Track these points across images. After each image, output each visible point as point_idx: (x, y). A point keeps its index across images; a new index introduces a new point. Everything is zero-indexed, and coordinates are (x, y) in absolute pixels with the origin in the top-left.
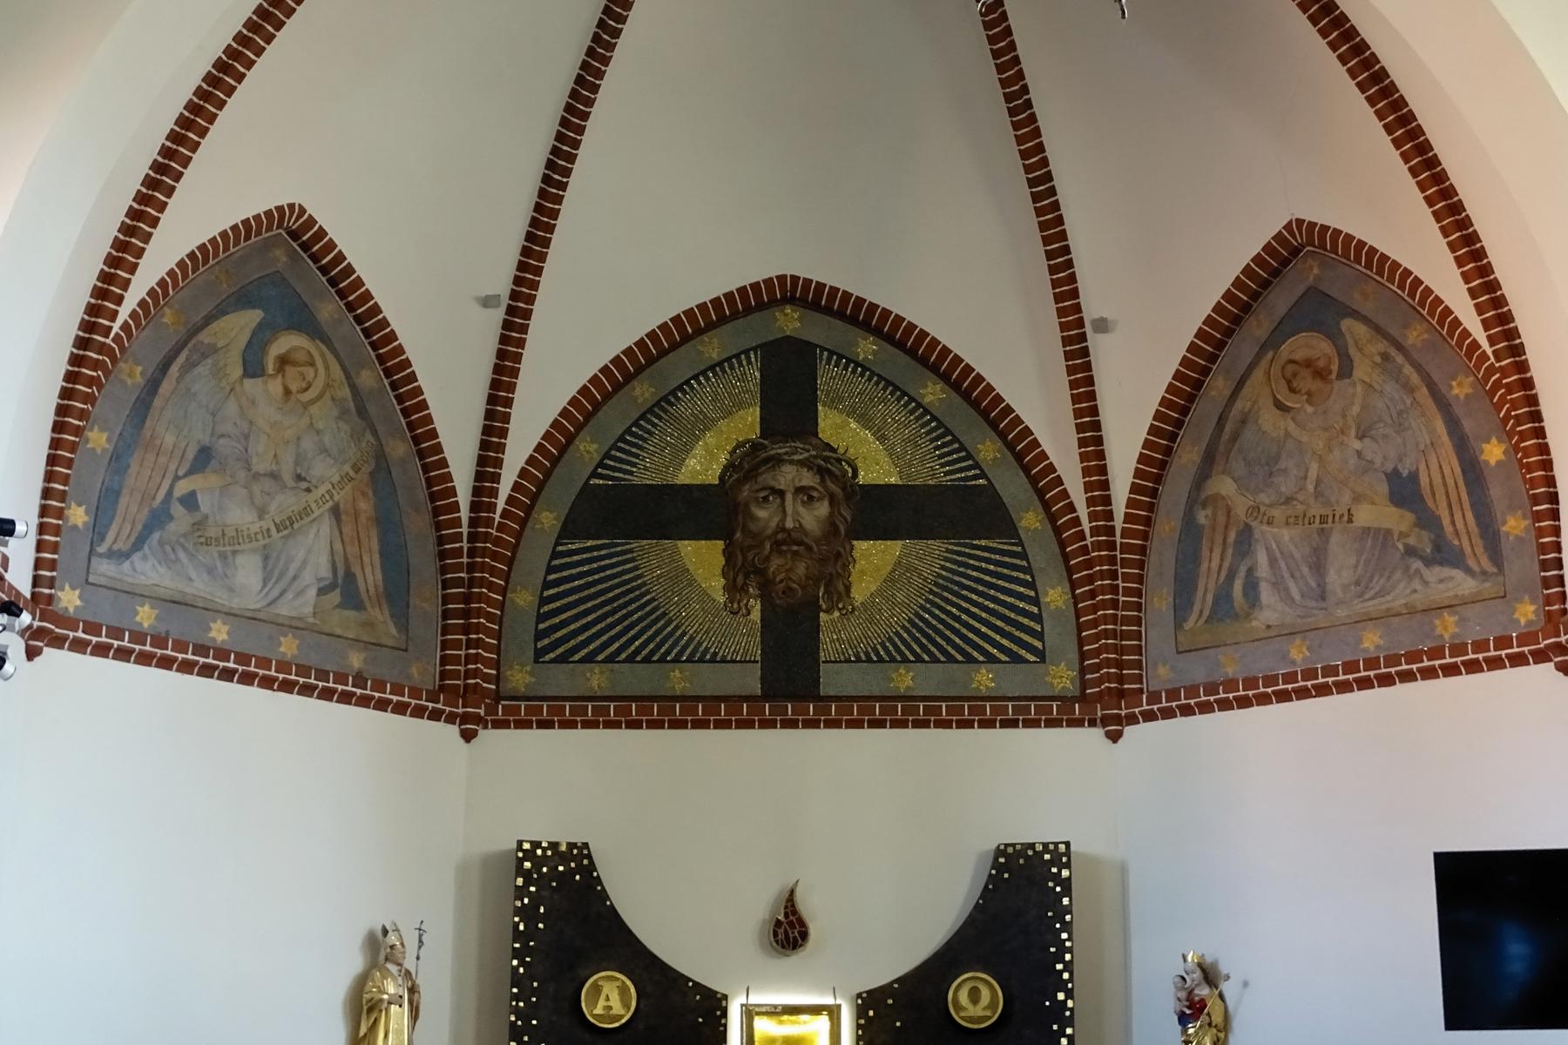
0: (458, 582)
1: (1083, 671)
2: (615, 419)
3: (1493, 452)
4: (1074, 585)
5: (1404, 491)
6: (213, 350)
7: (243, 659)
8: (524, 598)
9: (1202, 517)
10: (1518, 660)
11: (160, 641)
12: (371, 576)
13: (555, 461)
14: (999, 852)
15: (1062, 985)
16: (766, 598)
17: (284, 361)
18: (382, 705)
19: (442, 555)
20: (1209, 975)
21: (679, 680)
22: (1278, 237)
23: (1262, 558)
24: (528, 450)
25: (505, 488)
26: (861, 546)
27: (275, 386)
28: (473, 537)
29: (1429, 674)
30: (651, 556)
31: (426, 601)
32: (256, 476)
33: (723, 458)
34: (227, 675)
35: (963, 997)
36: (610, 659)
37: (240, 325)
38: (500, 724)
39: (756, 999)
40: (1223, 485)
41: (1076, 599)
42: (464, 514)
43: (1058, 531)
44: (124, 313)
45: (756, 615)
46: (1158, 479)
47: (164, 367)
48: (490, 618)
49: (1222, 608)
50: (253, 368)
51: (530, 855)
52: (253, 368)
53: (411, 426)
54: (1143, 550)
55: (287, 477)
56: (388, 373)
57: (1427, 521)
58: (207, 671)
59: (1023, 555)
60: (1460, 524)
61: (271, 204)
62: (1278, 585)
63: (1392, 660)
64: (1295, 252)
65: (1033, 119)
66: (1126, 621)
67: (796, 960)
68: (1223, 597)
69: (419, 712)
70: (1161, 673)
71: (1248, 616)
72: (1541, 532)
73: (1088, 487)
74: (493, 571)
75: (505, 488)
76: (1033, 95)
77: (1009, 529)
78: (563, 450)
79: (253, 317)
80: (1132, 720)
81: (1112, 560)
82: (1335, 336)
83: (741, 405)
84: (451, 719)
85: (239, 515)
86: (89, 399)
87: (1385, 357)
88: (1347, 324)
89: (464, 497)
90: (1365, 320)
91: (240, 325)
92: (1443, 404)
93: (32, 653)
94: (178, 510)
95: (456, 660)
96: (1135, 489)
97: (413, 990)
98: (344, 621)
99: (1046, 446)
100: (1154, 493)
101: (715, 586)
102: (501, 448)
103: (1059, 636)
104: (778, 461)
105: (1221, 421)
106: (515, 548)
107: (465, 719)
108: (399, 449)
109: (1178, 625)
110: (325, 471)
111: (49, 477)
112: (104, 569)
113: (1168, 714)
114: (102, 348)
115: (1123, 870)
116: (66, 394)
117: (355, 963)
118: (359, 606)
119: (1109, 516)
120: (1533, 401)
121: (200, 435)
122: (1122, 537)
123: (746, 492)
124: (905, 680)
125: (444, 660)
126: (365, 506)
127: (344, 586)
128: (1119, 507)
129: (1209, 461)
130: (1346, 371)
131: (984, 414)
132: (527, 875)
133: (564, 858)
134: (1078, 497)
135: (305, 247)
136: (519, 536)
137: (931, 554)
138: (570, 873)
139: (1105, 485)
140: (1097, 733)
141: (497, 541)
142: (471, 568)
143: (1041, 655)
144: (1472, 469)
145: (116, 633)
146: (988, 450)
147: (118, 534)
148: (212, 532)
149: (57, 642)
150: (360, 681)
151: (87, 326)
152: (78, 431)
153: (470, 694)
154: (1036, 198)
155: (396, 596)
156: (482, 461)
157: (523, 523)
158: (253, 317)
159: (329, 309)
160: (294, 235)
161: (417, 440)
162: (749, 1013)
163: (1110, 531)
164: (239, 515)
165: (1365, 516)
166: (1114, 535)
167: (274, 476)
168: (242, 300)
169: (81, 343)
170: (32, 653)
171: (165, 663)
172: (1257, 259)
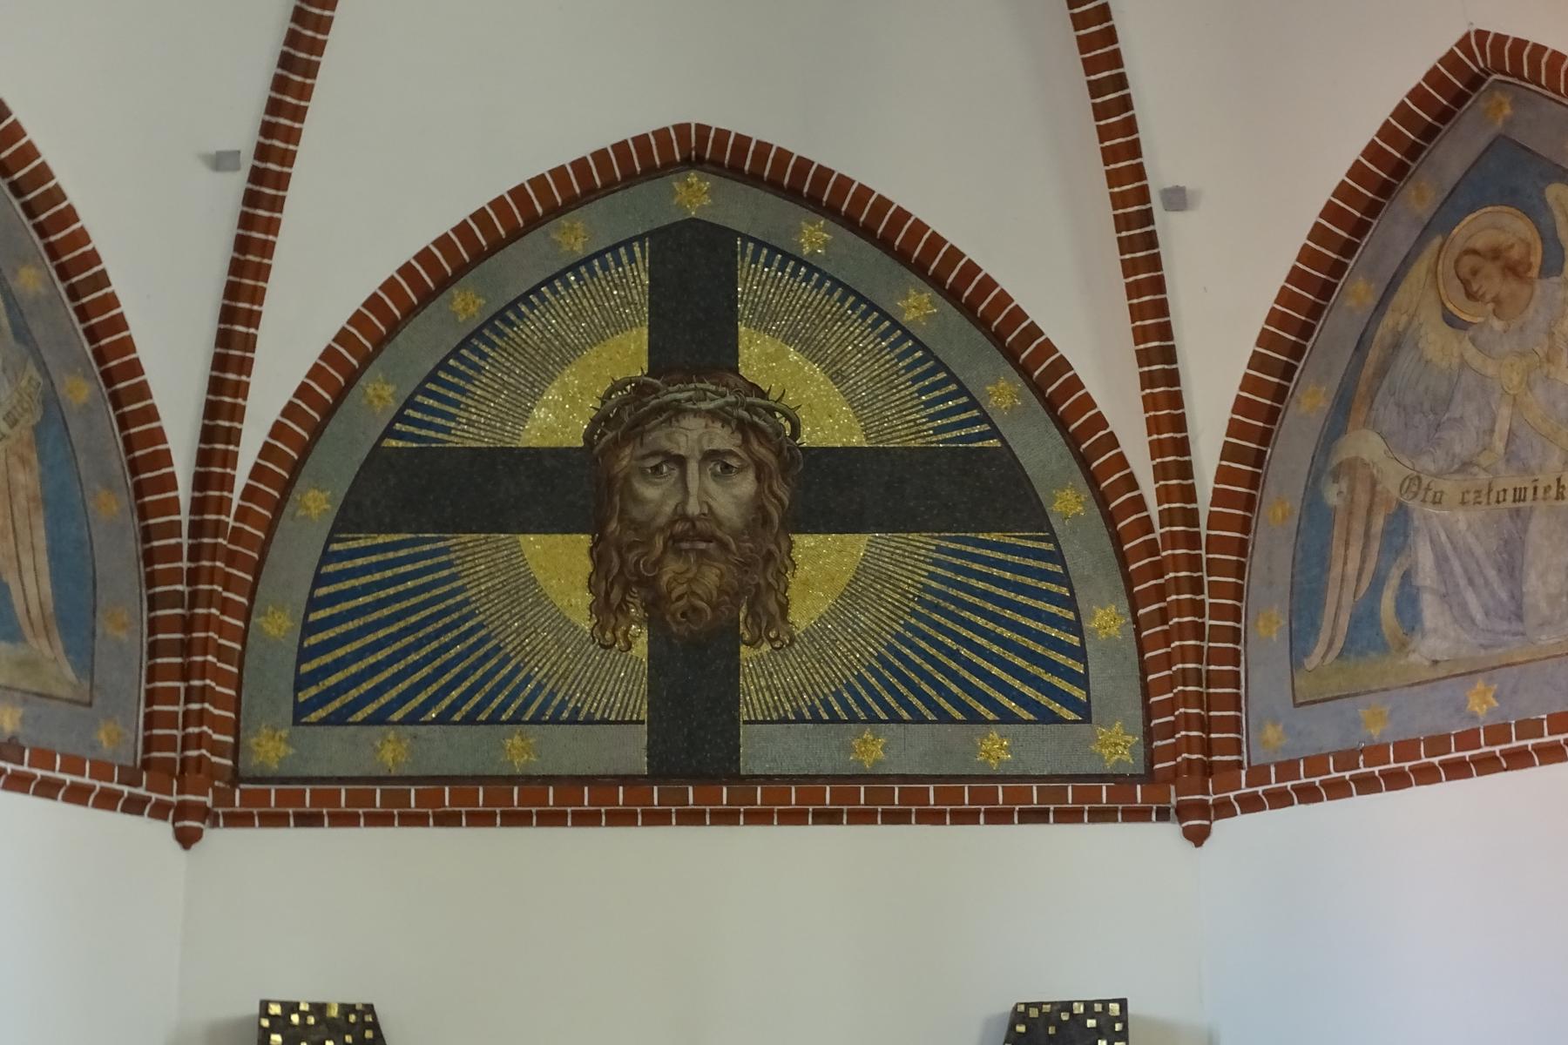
0: (174, 599)
1: (1149, 735)
9: (1333, 495)
14: (1018, 1016)
16: (656, 624)
19: (149, 557)
22: (1450, 60)
23: (1425, 558)
24: (286, 394)
25: (248, 452)
28: (197, 529)
33: (591, 405)
36: (412, 719)
38: (238, 820)
40: (1364, 445)
42: (184, 492)
45: (641, 648)
46: (1265, 437)
51: (280, 1024)
54: (1242, 548)
59: (1057, 557)
62: (1447, 597)
64: (1475, 82)
66: (1216, 656)
68: (1365, 618)
69: (107, 801)
75: (248, 452)
77: (1029, 511)
78: (341, 395)
80: (1224, 810)
84: (160, 811)
89: (183, 467)
96: (1229, 452)
101: (577, 604)
102: (241, 390)
104: (676, 411)
105: (1362, 345)
107: (182, 811)
109: (1296, 663)
119: (1189, 494)
123: (626, 458)
125: (151, 719)
128: (1205, 480)
134: (1142, 465)
139: (1183, 447)
156: (212, 410)
161: (109, 378)
163: (1191, 517)
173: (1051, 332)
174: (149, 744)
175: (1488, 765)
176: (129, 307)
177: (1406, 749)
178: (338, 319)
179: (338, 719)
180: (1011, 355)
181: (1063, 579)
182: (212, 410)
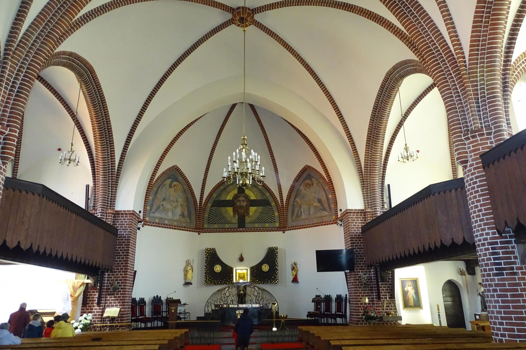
0: (198, 214)
1: (280, 224)
2: (218, 191)
3: (330, 196)
4: (279, 212)
5: (320, 201)
6: (165, 185)
7: (170, 225)
8: (206, 215)
9: (295, 204)
10: (332, 224)
11: (159, 224)
12: (186, 213)
13: (210, 197)
14: (269, 248)
15: (277, 266)
16: (238, 214)
17: (174, 186)
18: (188, 231)
19: (196, 210)
20: (295, 264)
21: (227, 226)
22: (304, 167)
23: (302, 209)
24: (207, 196)
25: (204, 201)
26: (251, 208)
27: (173, 189)
28: (199, 208)
29: (322, 225)
30: (223, 209)
31: (193, 217)
32: (171, 201)
33: (233, 196)
34: (168, 228)
35: (264, 267)
36: (218, 223)
37: (169, 181)
38: (203, 232)
39: (237, 268)
40: (297, 199)
41: (279, 214)
42: (198, 204)
43: (277, 205)
44: (155, 180)
45: (237, 217)
46: (289, 198)
47: (159, 188)
48: (202, 214)
49: (297, 216)
50: (170, 187)
51: (207, 250)
52: (170, 187)
53: (191, 193)
54: (288, 208)
55: (175, 201)
56: (188, 186)
57: (322, 205)
58: (165, 227)
59: (272, 209)
60: (326, 206)
61: (172, 165)
62: (304, 213)
63: (317, 223)
64: (306, 169)
65: (272, 152)
66: (285, 217)
67: (242, 262)
68: (298, 214)
69: (192, 231)
70: (290, 223)
71: (301, 217)
72: (335, 207)
73: (280, 200)
74: (202, 212)
75: (204, 201)
76: (272, 149)
77: (270, 205)
78: (211, 195)
79: (171, 180)
80: (286, 230)
81: (284, 209)
82: (311, 180)
83: (235, 189)
84: (197, 232)
85: (169, 206)
86: (149, 193)
87: (317, 183)
88: (313, 179)
89: (198, 202)
90: (315, 179)
91: (169, 181)
92: (324, 190)
93: (143, 226)
94: (161, 206)
95: (197, 224)
96: (286, 200)
97: (192, 268)
98: (183, 220)
99: (275, 194)
100: (289, 200)
101: (232, 213)
102: (203, 196)
103: (277, 219)
104: (240, 197)
105: (297, 191)
106: (205, 209)
107: (199, 232)
108: (190, 196)
109: (292, 218)
110: (180, 200)
111: (145, 203)
112: (152, 215)
113: (290, 230)
114: (152, 184)
115: (285, 251)
116: (147, 193)
117: (184, 265)
118: (185, 218)
119: (283, 203)
120: (334, 190)
121: (164, 196)
122: (456, 55)
123: (235, 201)
124: (256, 225)
125: (196, 224)
126: (185, 204)
127: (183, 215)
128: (284, 202)
129: (296, 196)
130: (313, 185)
131: (267, 190)
132: (207, 252)
133: (212, 250)
134: (279, 201)
135: (177, 170)
136: (206, 207)
137: (260, 209)
138: (212, 252)
139: (283, 199)
140: (282, 232)
141: (203, 208)
142: (199, 212)
143: (274, 222)
144: (328, 199)
145: (153, 223)
146: (268, 194)
147: (153, 210)
148: (165, 209)
149: (146, 225)
150: (185, 228)
151: (150, 182)
152: (148, 197)
153: (200, 229)
154: (273, 162)
155: (190, 216)
156: (201, 198)
157: (206, 205)
158: (171, 180)
159: (180, 178)
160: (175, 169)
161: (192, 195)
162: (236, 270)
163: (283, 205)
164: (169, 206)
165: (315, 204)
166: (454, 56)
167: (173, 201)
168: (169, 178)
169: (149, 184)
170: (143, 226)
171: (160, 227)
172: (302, 170)
173: (271, 189)
174: (196, 226)
175: (307, 227)
176: (194, 189)
177: (300, 226)
178: (211, 189)
179: (211, 223)
180: (268, 191)
181: (273, 210)
182: (201, 198)
